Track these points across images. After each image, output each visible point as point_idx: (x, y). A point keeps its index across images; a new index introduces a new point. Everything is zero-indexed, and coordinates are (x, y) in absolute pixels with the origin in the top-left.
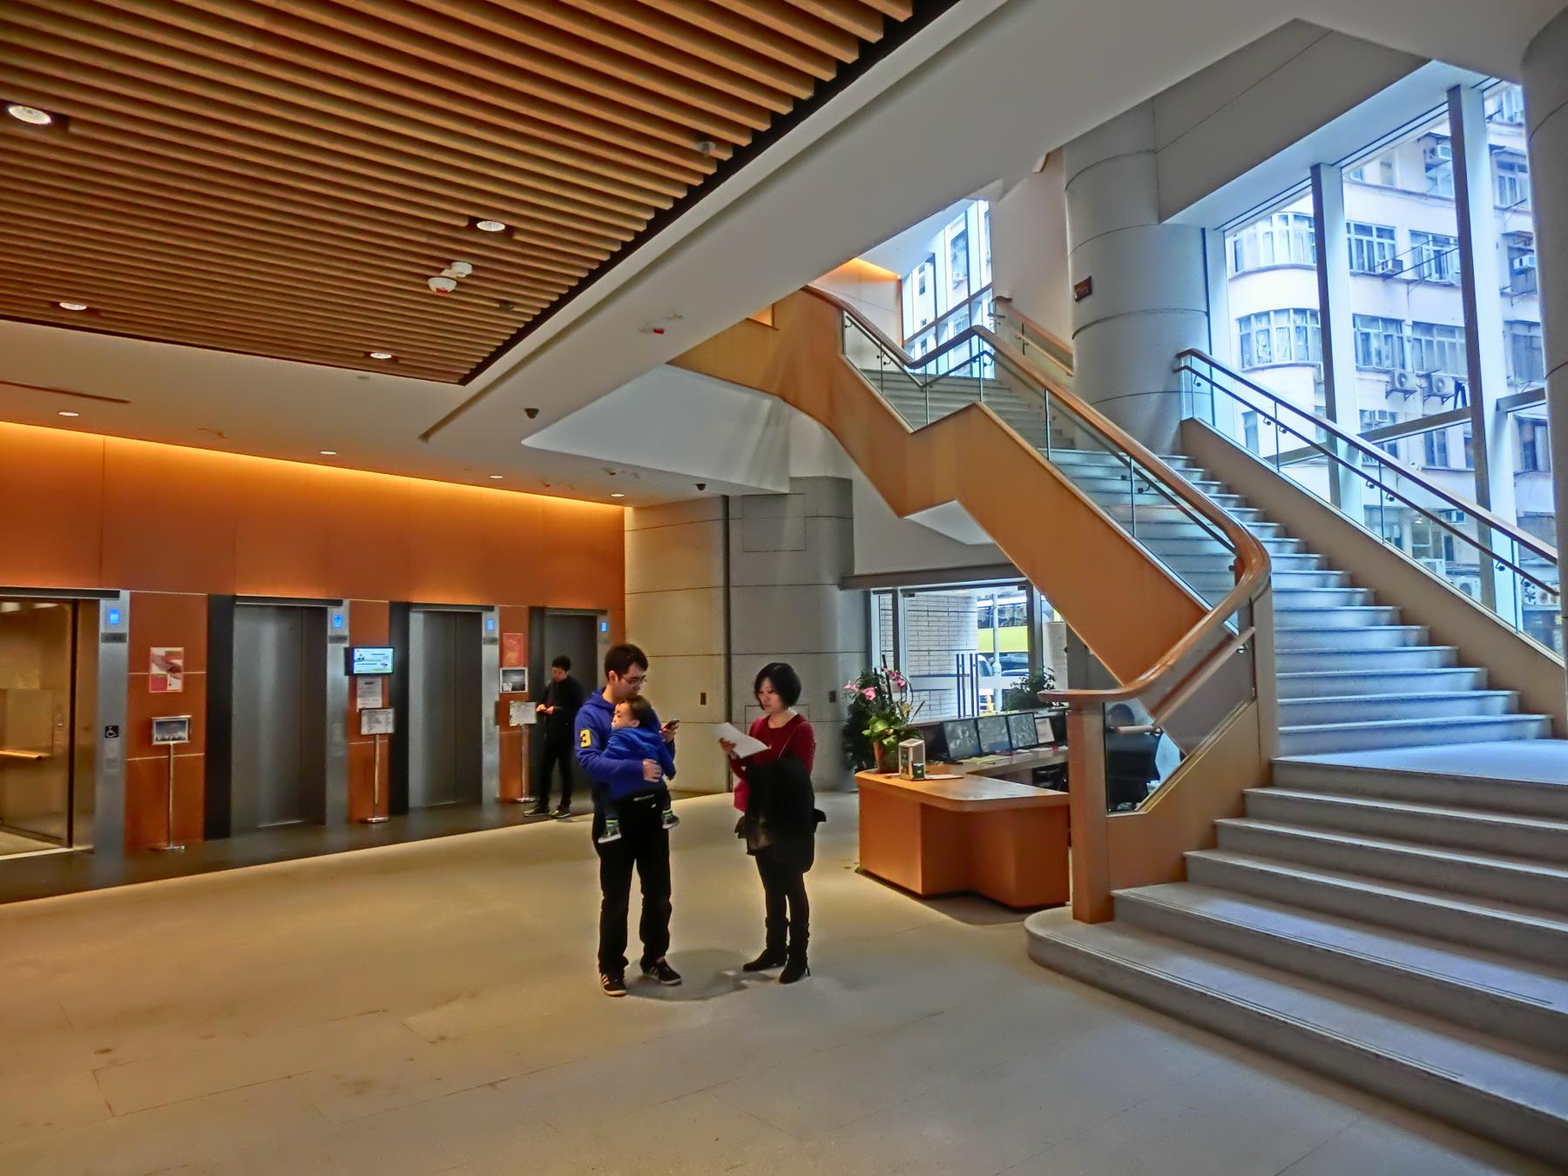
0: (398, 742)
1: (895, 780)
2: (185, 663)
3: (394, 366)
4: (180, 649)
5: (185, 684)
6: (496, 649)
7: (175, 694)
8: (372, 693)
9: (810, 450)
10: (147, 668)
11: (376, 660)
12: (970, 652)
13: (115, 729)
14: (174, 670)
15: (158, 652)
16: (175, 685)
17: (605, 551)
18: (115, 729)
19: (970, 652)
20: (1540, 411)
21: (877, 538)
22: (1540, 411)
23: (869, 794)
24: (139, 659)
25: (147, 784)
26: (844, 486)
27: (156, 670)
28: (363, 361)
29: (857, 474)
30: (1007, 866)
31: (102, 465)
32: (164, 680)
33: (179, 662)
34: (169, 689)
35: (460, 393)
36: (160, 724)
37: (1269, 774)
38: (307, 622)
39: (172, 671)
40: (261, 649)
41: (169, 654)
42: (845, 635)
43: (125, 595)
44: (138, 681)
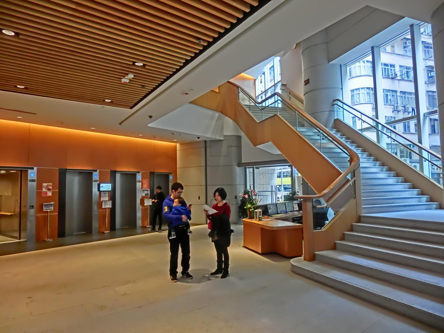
0: (113, 210)
1: (253, 221)
2: (52, 188)
3: (112, 104)
4: (51, 184)
5: (52, 194)
6: (140, 184)
7: (49, 196)
8: (105, 196)
9: (229, 127)
10: (42, 189)
11: (106, 187)
12: (275, 185)
13: (33, 206)
14: (49, 190)
15: (45, 184)
16: (50, 194)
17: (171, 156)
18: (33, 206)
19: (275, 185)
20: (436, 116)
21: (248, 152)
22: (436, 116)
23: (246, 225)
24: (39, 187)
25: (42, 222)
26: (239, 138)
27: (44, 190)
28: (103, 102)
29: (243, 134)
30: (285, 245)
31: (29, 132)
32: (46, 193)
33: (51, 188)
34: (48, 195)
35: (130, 111)
36: (45, 205)
37: (359, 219)
38: (87, 176)
39: (49, 190)
40: (74, 184)
41: (48, 185)
42: (239, 180)
43: (35, 168)
44: (39, 193)
